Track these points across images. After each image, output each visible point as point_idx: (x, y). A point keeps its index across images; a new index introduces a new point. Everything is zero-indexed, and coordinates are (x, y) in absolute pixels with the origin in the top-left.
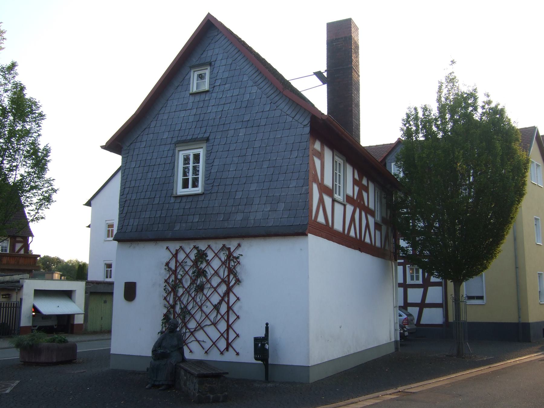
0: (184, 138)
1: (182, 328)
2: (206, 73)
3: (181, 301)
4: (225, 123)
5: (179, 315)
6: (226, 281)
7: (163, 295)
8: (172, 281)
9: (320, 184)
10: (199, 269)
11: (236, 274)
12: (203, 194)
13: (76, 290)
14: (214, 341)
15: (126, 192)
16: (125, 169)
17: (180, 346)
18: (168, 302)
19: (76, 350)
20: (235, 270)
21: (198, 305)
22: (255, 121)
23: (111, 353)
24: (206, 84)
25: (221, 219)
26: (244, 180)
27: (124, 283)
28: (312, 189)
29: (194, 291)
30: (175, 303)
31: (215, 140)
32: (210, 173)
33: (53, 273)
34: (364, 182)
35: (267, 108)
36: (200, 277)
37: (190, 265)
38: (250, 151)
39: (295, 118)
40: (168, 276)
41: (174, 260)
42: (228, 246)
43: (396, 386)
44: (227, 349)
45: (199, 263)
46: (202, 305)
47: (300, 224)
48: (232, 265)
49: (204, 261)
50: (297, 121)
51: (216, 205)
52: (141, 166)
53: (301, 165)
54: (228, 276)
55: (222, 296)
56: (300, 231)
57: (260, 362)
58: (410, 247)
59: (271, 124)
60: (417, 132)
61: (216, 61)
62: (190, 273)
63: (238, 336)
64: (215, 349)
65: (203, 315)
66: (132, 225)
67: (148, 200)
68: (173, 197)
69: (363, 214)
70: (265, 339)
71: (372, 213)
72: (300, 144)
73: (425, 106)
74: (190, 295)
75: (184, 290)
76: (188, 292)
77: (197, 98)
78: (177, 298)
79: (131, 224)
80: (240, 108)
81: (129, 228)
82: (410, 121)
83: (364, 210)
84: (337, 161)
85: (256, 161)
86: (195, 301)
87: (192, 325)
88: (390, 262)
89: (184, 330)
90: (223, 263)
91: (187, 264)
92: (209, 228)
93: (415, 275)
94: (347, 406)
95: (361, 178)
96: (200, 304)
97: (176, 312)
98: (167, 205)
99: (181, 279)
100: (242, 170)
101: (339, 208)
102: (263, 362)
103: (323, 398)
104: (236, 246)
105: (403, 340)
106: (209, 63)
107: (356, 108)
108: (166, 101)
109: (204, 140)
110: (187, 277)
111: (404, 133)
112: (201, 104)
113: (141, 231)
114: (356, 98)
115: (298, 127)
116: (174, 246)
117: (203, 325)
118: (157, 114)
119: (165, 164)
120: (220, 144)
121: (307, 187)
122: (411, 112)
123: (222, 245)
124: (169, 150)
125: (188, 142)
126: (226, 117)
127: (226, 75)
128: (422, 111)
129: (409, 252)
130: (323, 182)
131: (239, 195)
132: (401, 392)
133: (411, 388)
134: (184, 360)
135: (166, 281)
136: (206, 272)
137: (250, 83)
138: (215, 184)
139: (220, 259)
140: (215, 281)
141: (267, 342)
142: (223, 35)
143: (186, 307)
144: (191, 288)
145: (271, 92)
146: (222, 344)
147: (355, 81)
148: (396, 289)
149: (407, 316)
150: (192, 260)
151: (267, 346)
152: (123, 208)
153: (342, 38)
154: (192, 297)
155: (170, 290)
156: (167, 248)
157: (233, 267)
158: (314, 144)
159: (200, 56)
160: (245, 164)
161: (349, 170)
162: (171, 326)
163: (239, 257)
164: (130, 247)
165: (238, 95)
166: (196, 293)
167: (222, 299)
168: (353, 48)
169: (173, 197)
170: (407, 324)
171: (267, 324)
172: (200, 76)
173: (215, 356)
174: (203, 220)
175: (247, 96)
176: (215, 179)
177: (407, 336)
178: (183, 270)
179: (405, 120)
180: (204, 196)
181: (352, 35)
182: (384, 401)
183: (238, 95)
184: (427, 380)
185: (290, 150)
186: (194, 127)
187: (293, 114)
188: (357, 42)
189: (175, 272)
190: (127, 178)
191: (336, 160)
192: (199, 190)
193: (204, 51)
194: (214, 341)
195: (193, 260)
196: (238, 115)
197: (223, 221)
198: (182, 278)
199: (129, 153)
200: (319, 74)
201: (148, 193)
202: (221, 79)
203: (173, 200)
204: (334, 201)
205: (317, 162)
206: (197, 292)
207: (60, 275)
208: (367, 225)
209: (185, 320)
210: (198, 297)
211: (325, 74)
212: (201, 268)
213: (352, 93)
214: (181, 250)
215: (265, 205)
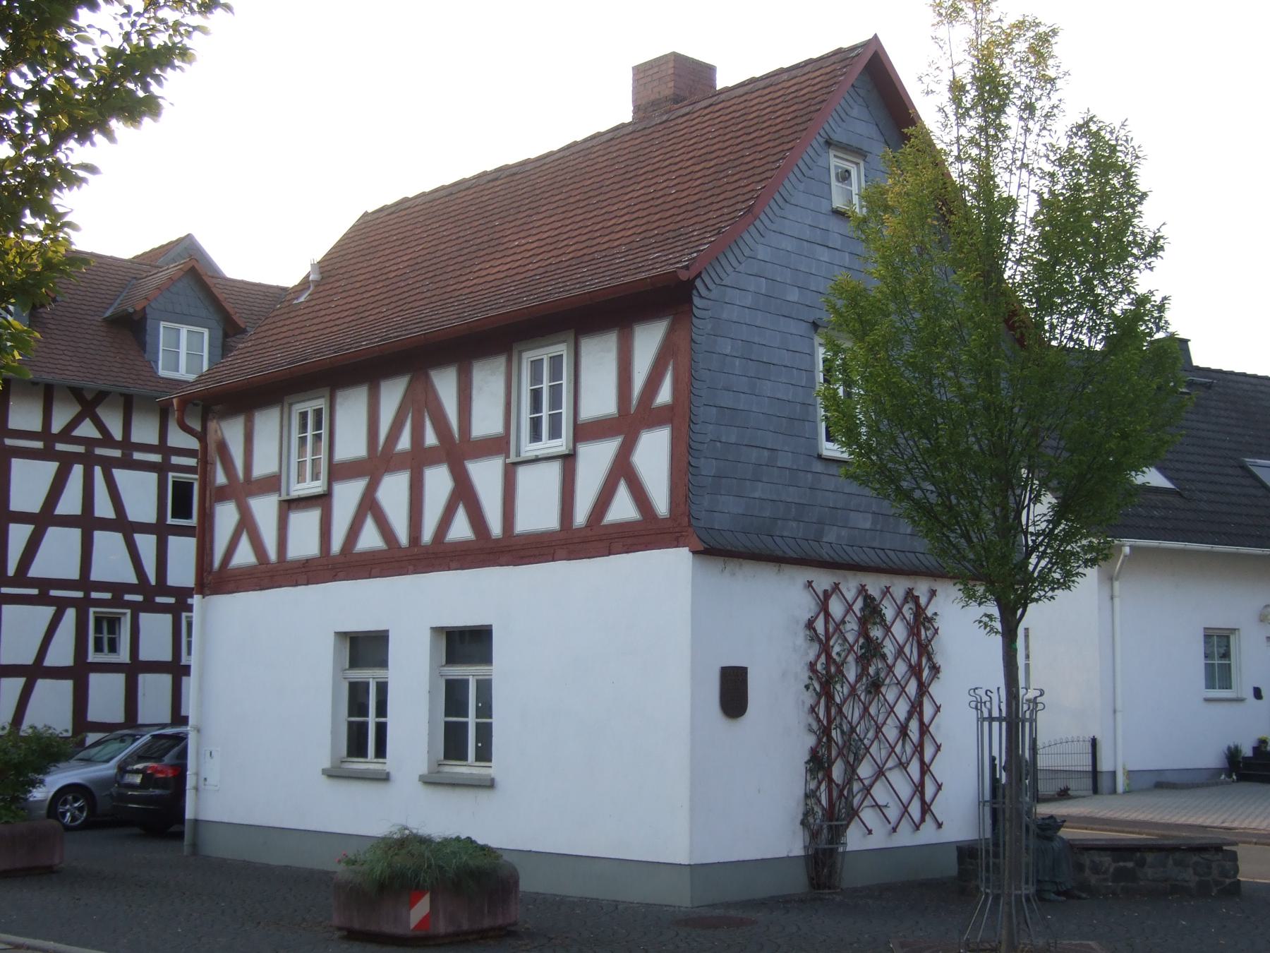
116: (823, 580)
146: (915, 809)
171: (1094, 742)
173: (905, 837)
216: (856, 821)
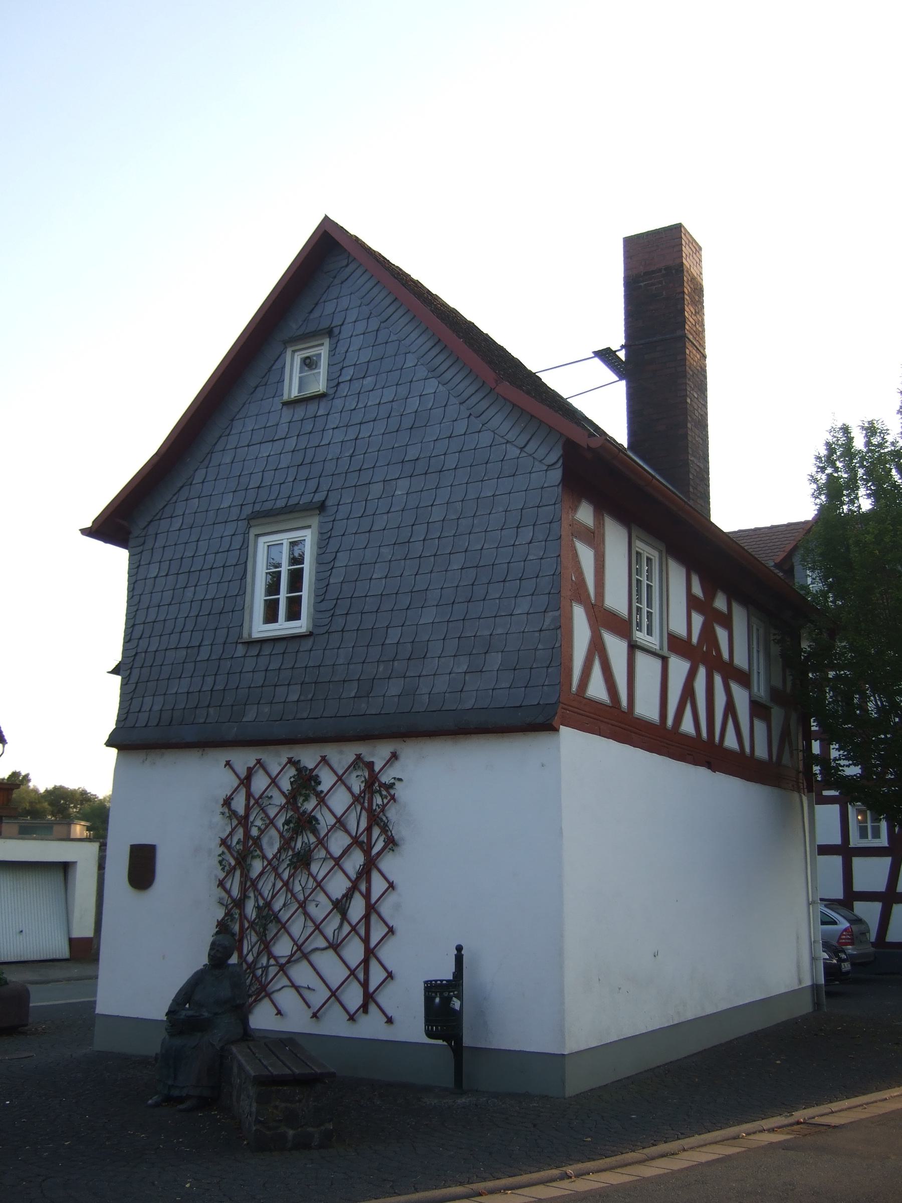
0: (268, 506)
1: (259, 954)
2: (321, 354)
3: (258, 891)
4: (363, 468)
5: (252, 924)
6: (363, 842)
7: (216, 876)
8: (238, 843)
9: (593, 606)
10: (301, 814)
11: (386, 825)
12: (310, 635)
13: (76, 862)
14: (334, 988)
15: (137, 634)
16: (136, 581)
17: (238, 1002)
18: (228, 892)
19: (29, 1003)
20: (385, 816)
21: (297, 900)
22: (432, 460)
23: (96, 1012)
24: (320, 379)
25: (353, 694)
26: (405, 601)
27: (129, 846)
28: (570, 619)
29: (288, 865)
30: (244, 897)
31: (339, 507)
32: (327, 585)
33: (69, 824)
34: (720, 603)
35: (461, 427)
36: (302, 832)
37: (279, 804)
38: (421, 530)
39: (525, 450)
40: (229, 829)
41: (243, 792)
42: (368, 759)
43: (789, 1106)
44: (365, 1008)
45: (301, 800)
46: (306, 899)
47: (538, 704)
48: (377, 805)
49: (312, 795)
50: (530, 455)
51: (341, 661)
52: (169, 574)
53: (543, 561)
54: (369, 829)
55: (353, 879)
56: (540, 719)
57: (440, 1042)
58: (844, 759)
59: (470, 466)
60: (852, 485)
61: (342, 324)
62: (280, 822)
63: (390, 975)
64: (337, 1007)
65: (310, 923)
66: (150, 710)
67: (184, 652)
68: (240, 645)
69: (718, 680)
70: (455, 984)
71: (744, 679)
72: (539, 509)
73: (871, 423)
74: (278, 876)
75: (266, 863)
76: (275, 869)
77: (300, 412)
78: (249, 884)
79: (146, 707)
80: (397, 431)
81: (143, 717)
82: (836, 460)
83: (719, 671)
84: (642, 552)
85: (433, 553)
86: (290, 890)
87: (283, 948)
88: (796, 795)
89: (264, 961)
90: (357, 799)
91: (271, 803)
92: (325, 715)
93: (869, 825)
94: (646, 1163)
95: (710, 594)
96: (301, 897)
97: (246, 918)
98: (229, 663)
99: (259, 838)
100: (401, 576)
101: (647, 667)
102: (446, 1042)
103: (589, 1139)
104: (387, 758)
105: (837, 982)
106: (327, 330)
107: (697, 431)
108: (230, 422)
109: (312, 509)
110: (273, 832)
111: (819, 488)
112: (308, 427)
113: (169, 725)
114: (696, 407)
115: (534, 470)
116: (244, 759)
117: (308, 947)
118: (209, 453)
119: (224, 567)
120: (351, 516)
121: (557, 613)
122: (838, 440)
123: (355, 756)
124: (234, 535)
125: (278, 514)
126: (365, 453)
127: (365, 356)
128: (864, 435)
129: (840, 771)
130: (603, 601)
131: (394, 636)
132: (801, 1123)
133: (832, 1112)
134: (247, 1035)
135: (223, 842)
136: (317, 820)
137: (422, 372)
138: (338, 612)
139: (349, 789)
140: (338, 843)
141: (456, 993)
142: (359, 266)
143: (268, 904)
144: (281, 860)
145: (471, 390)
146: (353, 997)
147: (693, 368)
148: (814, 863)
149: (851, 924)
150: (283, 793)
151: (456, 1004)
152: (129, 671)
153: (660, 270)
154: (282, 880)
155: (233, 863)
156: (228, 764)
157: (379, 808)
158: (575, 509)
159: (307, 315)
160: (408, 562)
161: (677, 575)
162: (215, 951)
163: (394, 784)
164: (143, 762)
165: (393, 401)
166: (292, 871)
167: (354, 888)
168: (686, 291)
169: (242, 643)
170: (852, 944)
171: (459, 948)
172: (308, 361)
174: (310, 697)
175: (414, 404)
176: (338, 599)
177: (848, 973)
178: (263, 815)
179: (823, 459)
180: (311, 639)
181: (684, 261)
182: (749, 1150)
183: (393, 401)
184: (878, 1090)
185: (516, 525)
186: (290, 479)
187: (521, 442)
188: (698, 278)
189: (244, 821)
190: (139, 602)
191: (637, 549)
192: (301, 626)
193: (317, 304)
194: (334, 988)
195: (287, 792)
196: (393, 448)
197: (356, 699)
198: (261, 835)
199: (144, 543)
200: (606, 355)
201: (186, 636)
202: (355, 365)
203: (241, 650)
204: (633, 647)
205: (586, 555)
206: (296, 869)
207: (85, 827)
208: (730, 708)
209: (267, 936)
210: (297, 882)
211: (622, 355)
212: (305, 812)
213: (686, 396)
214: (258, 767)
215: (456, 658)
216: (266, 1003)
